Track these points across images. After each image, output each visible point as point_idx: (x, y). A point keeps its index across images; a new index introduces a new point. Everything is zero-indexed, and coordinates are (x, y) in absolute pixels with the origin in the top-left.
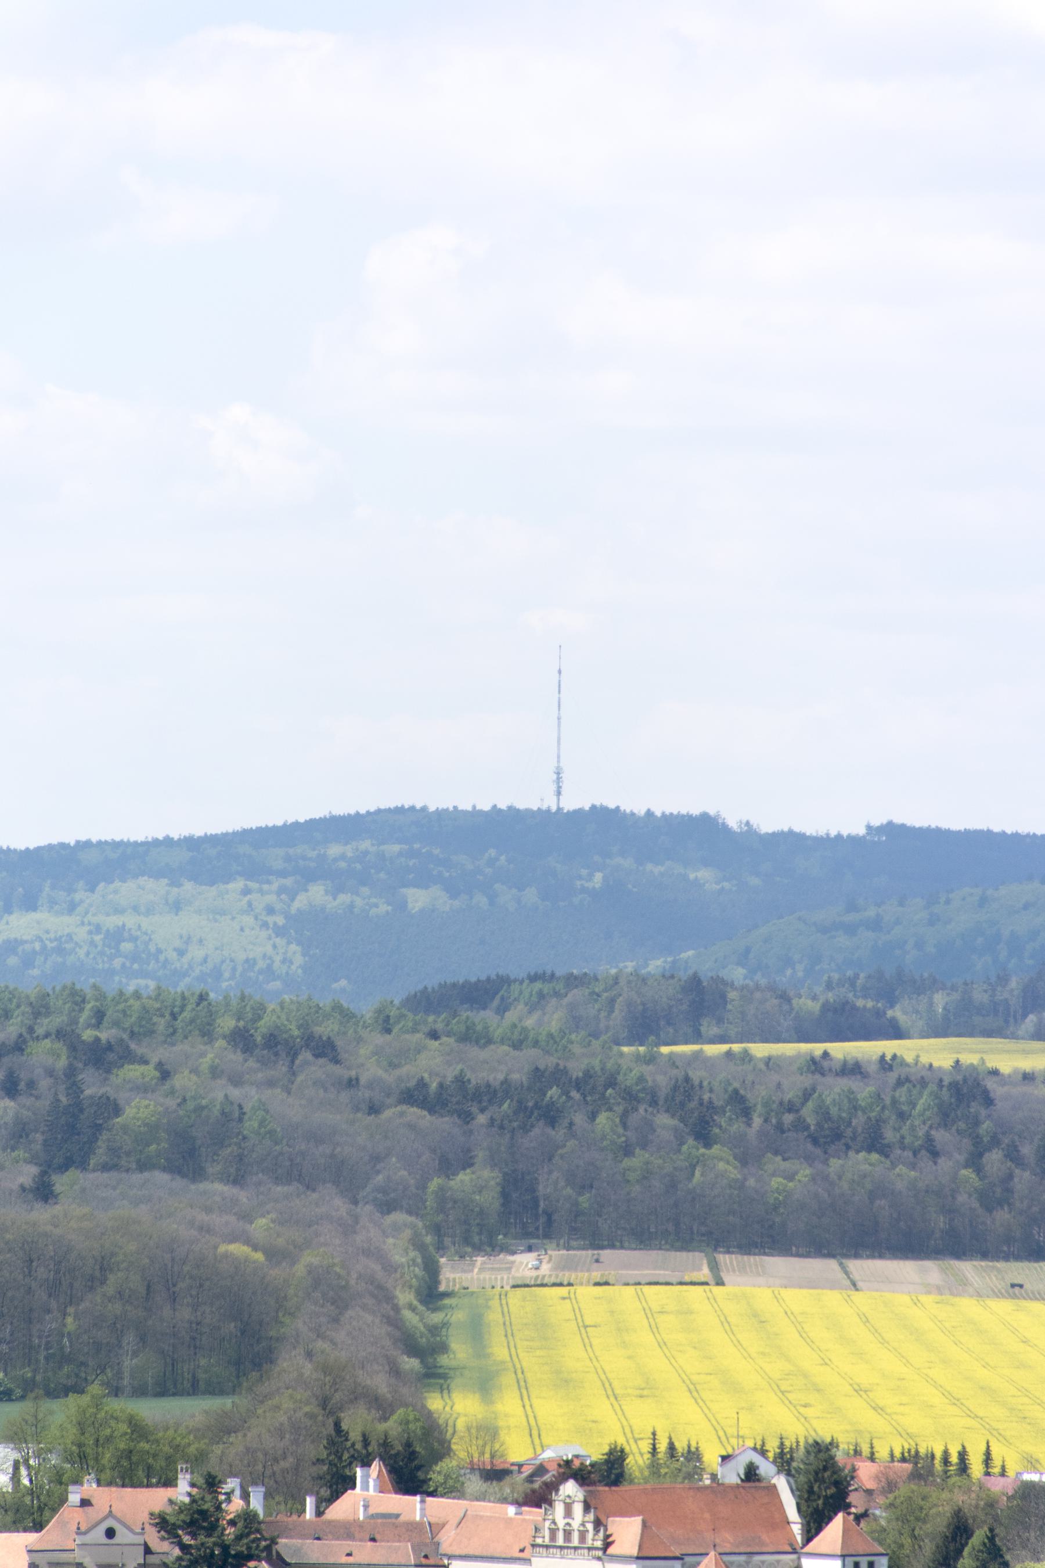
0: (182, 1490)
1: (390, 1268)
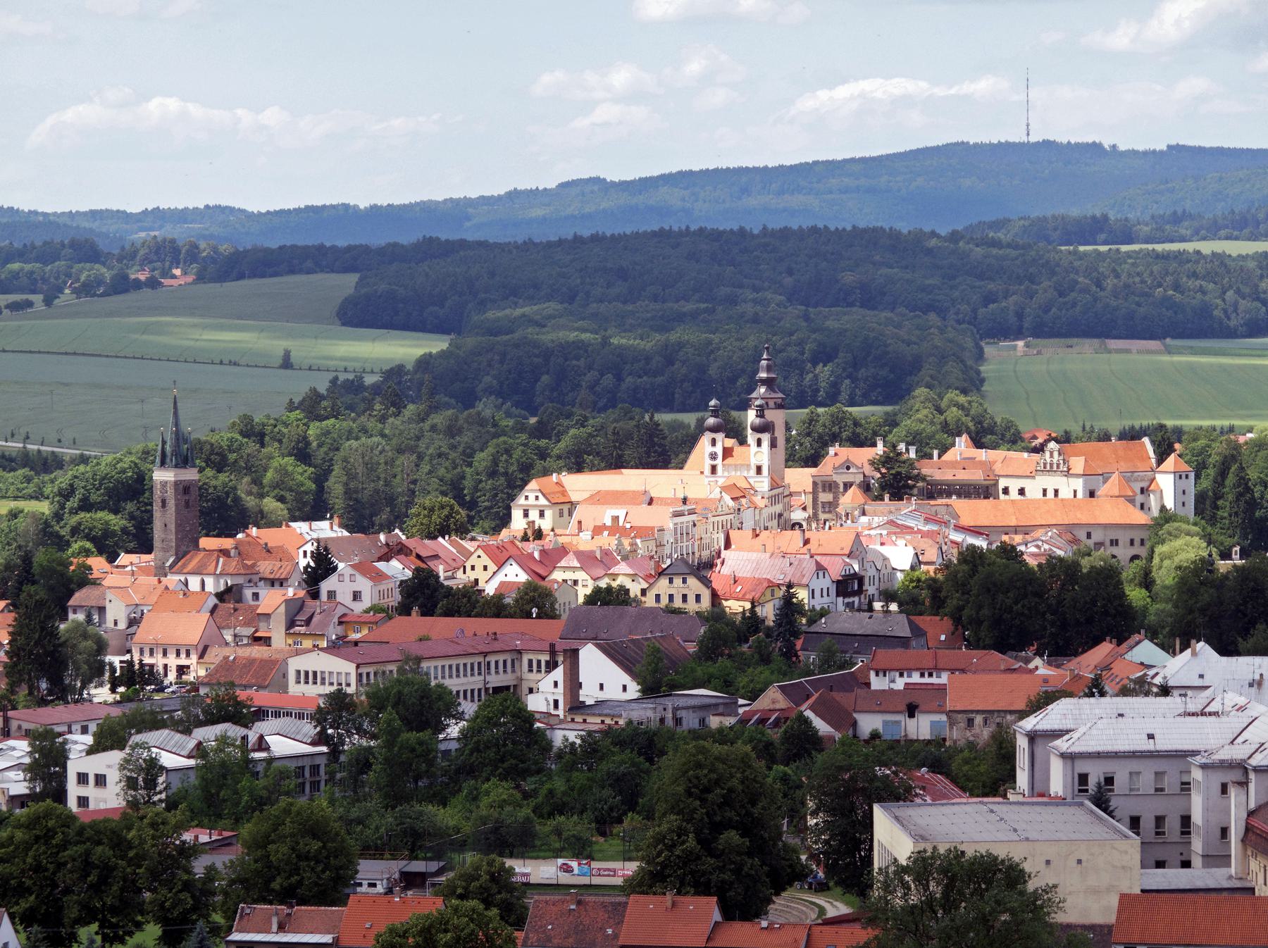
0: (880, 448)
1: (963, 349)
